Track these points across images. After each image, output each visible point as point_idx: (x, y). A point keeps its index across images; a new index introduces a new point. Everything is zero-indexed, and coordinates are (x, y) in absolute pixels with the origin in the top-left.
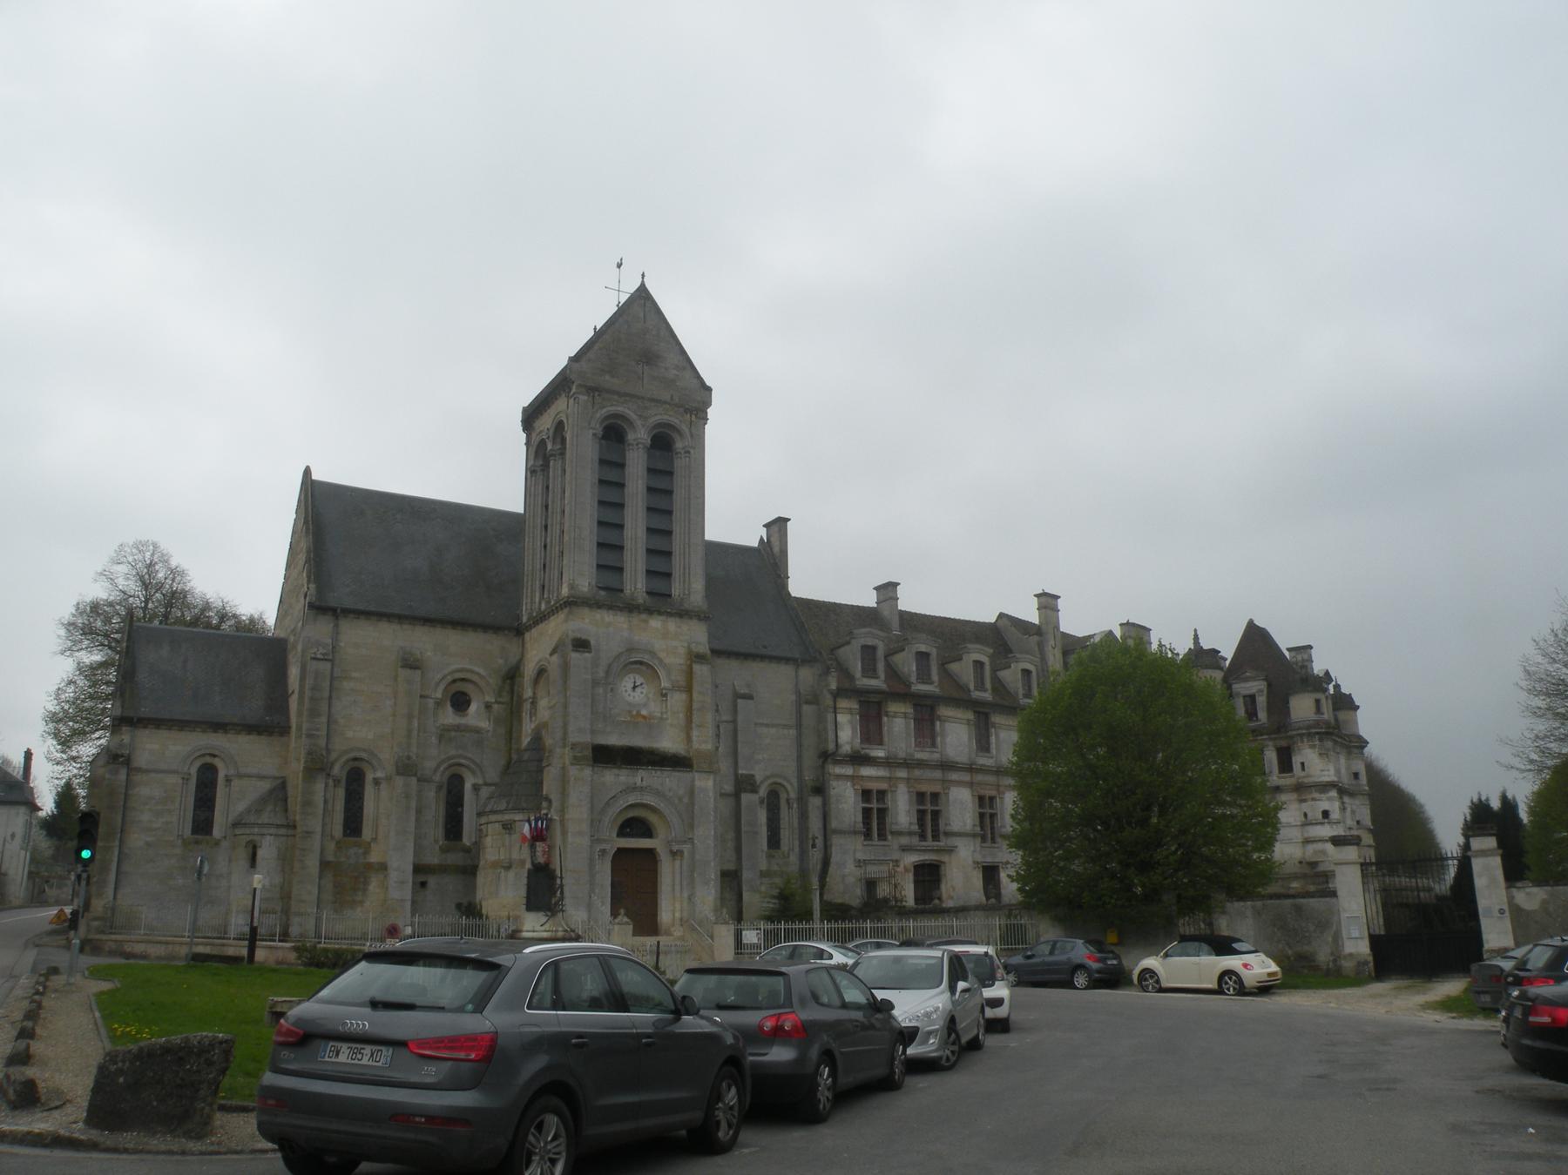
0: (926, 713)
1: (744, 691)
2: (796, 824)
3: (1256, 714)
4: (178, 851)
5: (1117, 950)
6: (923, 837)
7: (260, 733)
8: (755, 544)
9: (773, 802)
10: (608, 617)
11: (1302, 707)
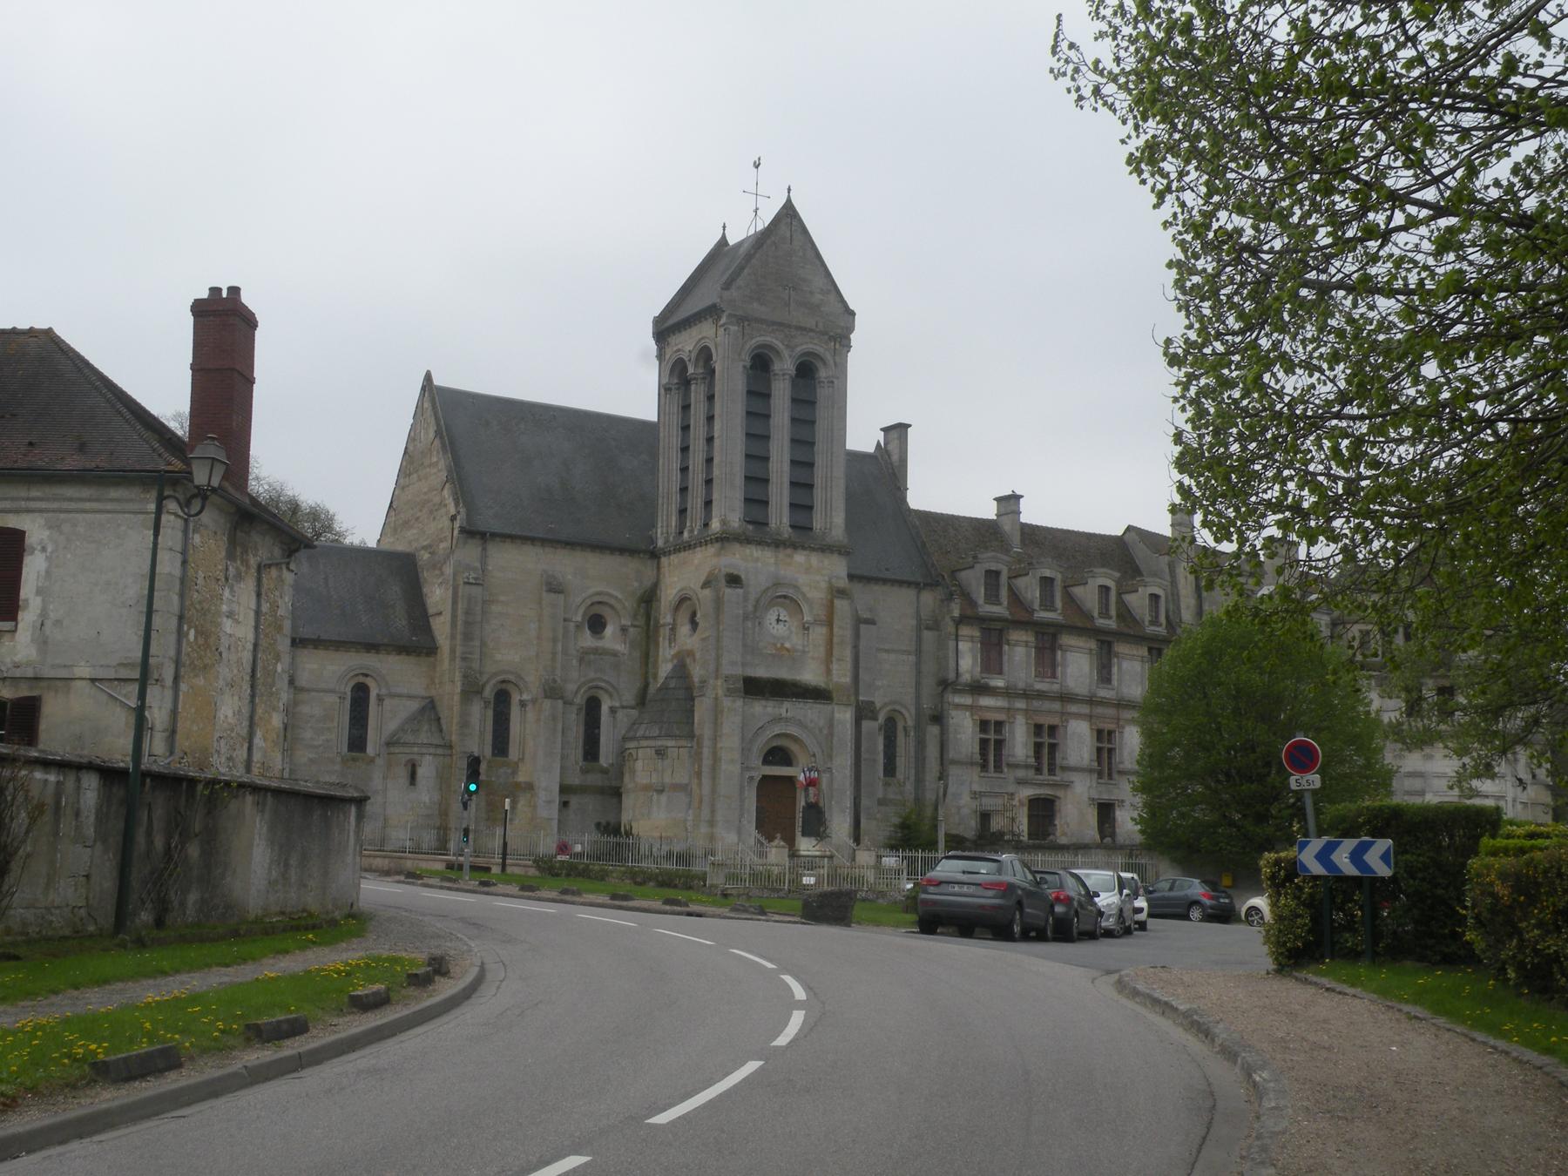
0: (1048, 641)
1: (866, 615)
2: (912, 753)
4: (337, 767)
5: (1230, 891)
6: (1038, 770)
7: (408, 653)
8: (871, 449)
10: (754, 552)
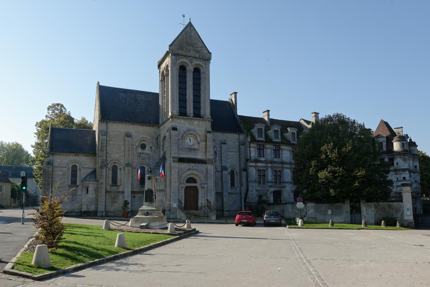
2: (239, 180)
3: (382, 148)
9: (232, 173)
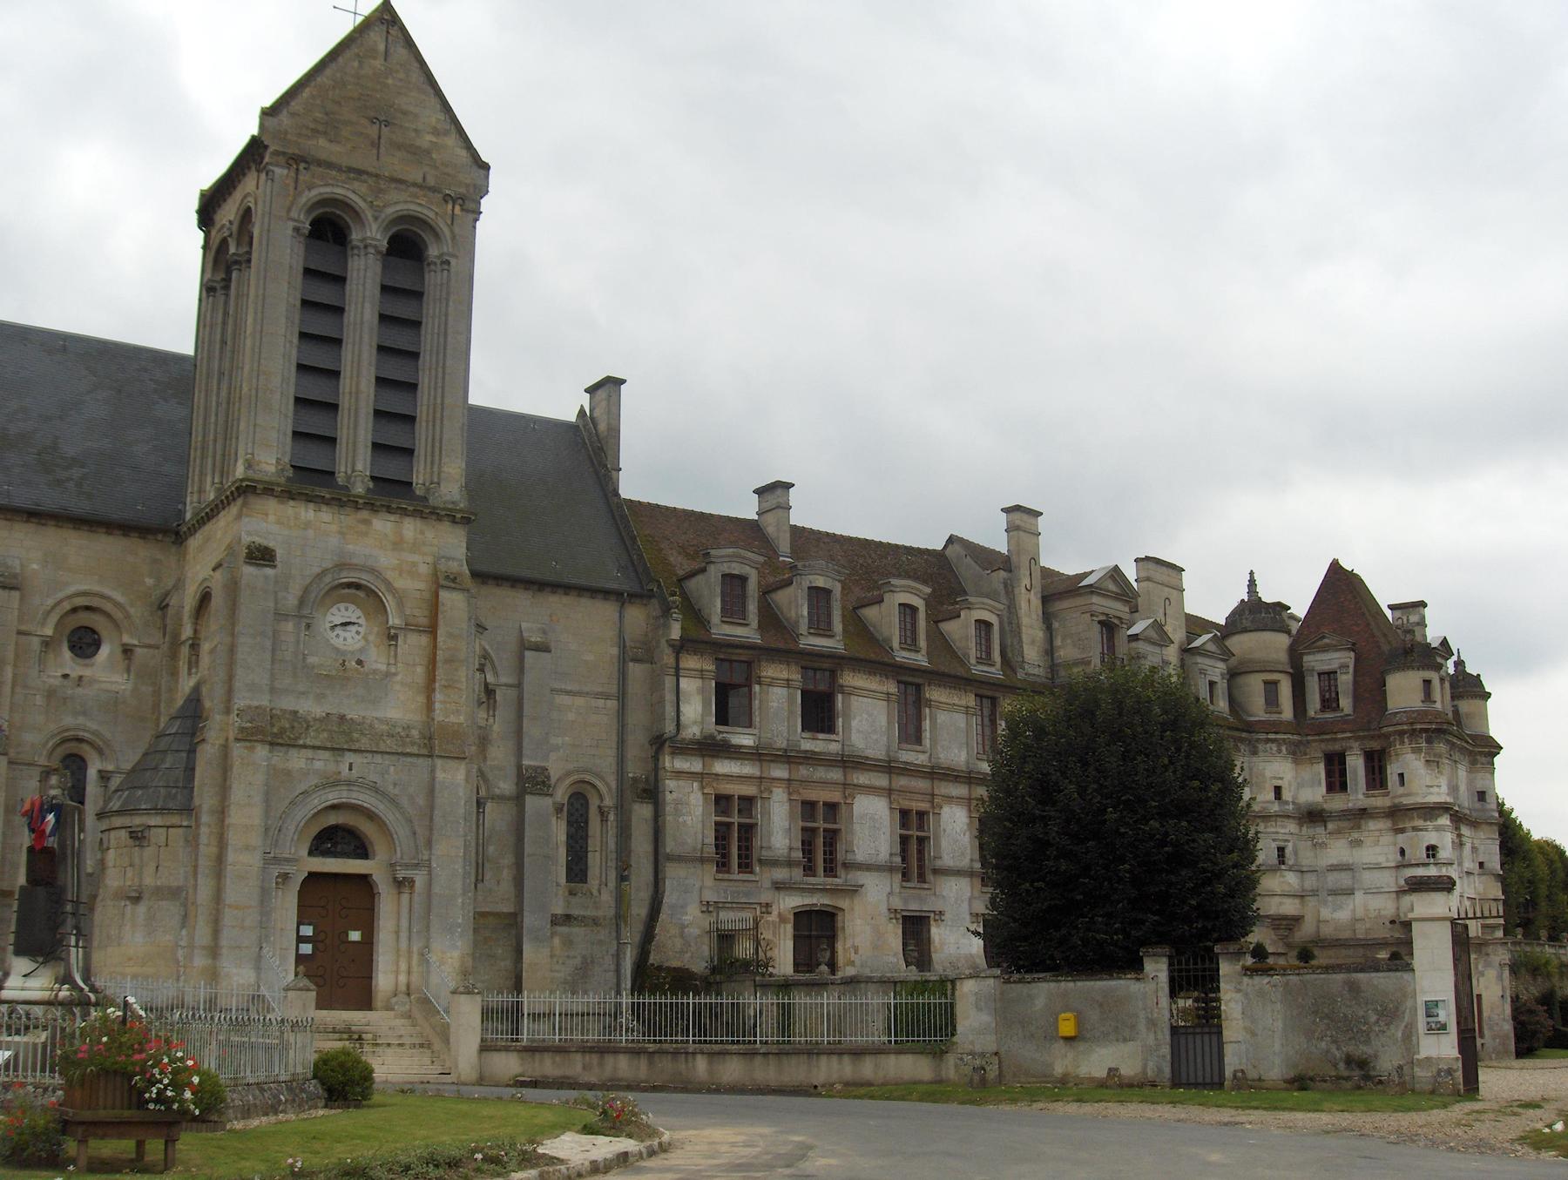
0: (912, 692)
1: (535, 638)
2: (612, 845)
6: (809, 869)
8: (571, 417)
9: (577, 812)
11: (1403, 690)
